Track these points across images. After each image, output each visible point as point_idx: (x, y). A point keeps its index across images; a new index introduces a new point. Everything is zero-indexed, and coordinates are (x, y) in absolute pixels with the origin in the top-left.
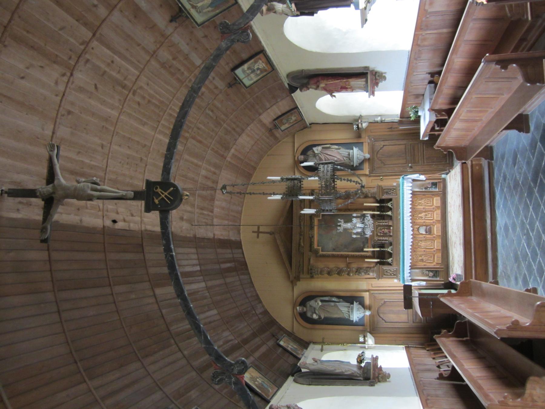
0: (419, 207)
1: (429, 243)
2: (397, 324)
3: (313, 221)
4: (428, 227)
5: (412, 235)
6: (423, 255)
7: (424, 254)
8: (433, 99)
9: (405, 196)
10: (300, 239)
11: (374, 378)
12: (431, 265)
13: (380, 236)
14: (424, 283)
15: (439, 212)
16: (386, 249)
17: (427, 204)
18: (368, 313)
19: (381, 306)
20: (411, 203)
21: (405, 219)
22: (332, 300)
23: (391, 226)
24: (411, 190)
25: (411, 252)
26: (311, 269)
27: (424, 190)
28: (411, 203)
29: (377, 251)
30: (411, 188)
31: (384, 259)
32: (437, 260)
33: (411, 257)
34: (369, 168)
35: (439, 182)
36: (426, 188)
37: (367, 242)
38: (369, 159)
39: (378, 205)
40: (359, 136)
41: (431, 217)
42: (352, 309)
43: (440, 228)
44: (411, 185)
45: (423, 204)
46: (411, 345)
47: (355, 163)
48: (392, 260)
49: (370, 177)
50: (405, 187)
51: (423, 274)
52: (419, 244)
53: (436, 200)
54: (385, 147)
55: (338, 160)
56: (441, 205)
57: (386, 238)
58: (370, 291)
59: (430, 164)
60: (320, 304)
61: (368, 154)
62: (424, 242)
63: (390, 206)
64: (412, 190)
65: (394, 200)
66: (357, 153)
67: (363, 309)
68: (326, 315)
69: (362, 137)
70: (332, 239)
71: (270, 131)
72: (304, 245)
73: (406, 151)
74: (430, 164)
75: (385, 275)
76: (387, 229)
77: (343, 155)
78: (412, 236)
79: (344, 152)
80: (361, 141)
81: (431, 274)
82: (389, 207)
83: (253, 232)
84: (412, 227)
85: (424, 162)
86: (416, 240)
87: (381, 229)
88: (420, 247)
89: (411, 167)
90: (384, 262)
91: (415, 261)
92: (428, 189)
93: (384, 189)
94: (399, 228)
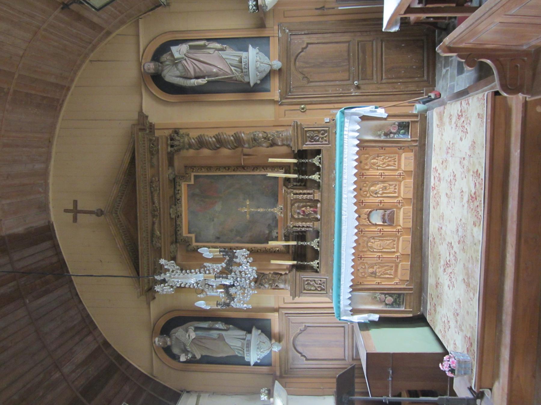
0: (372, 172)
1: (388, 242)
3: (178, 188)
4: (388, 212)
6: (376, 264)
7: (379, 263)
8: (177, 280)
9: (346, 151)
10: (153, 223)
12: (386, 284)
13: (298, 220)
14: (375, 317)
15: (410, 181)
16: (309, 243)
17: (388, 165)
18: (276, 348)
21: (344, 196)
22: (214, 327)
23: (318, 201)
24: (358, 138)
27: (383, 138)
29: (293, 245)
30: (357, 134)
32: (402, 275)
33: (353, 270)
34: (279, 89)
35: (412, 121)
36: (386, 135)
37: (276, 226)
38: (280, 70)
39: (295, 161)
40: (262, 25)
41: (395, 192)
42: (248, 345)
43: (411, 214)
44: (358, 127)
48: (318, 263)
49: (280, 105)
50: (345, 133)
51: (374, 300)
52: (369, 244)
53: (406, 158)
54: (309, 46)
55: (221, 73)
56: (415, 169)
57: (308, 224)
58: (280, 310)
59: (394, 81)
60: (193, 335)
61: (279, 60)
62: (380, 240)
63: (317, 164)
64: (359, 138)
65: (324, 152)
69: (267, 26)
70: (213, 221)
71: (62, 8)
72: (160, 233)
73: (349, 55)
74: (394, 81)
75: (305, 289)
76: (311, 207)
77: (228, 62)
78: (356, 231)
83: (66, 211)
84: (356, 211)
85: (382, 77)
86: (363, 236)
87: (299, 208)
88: (371, 249)
89: (358, 87)
91: (360, 276)
92: (392, 135)
93: (306, 131)
94: (333, 206)
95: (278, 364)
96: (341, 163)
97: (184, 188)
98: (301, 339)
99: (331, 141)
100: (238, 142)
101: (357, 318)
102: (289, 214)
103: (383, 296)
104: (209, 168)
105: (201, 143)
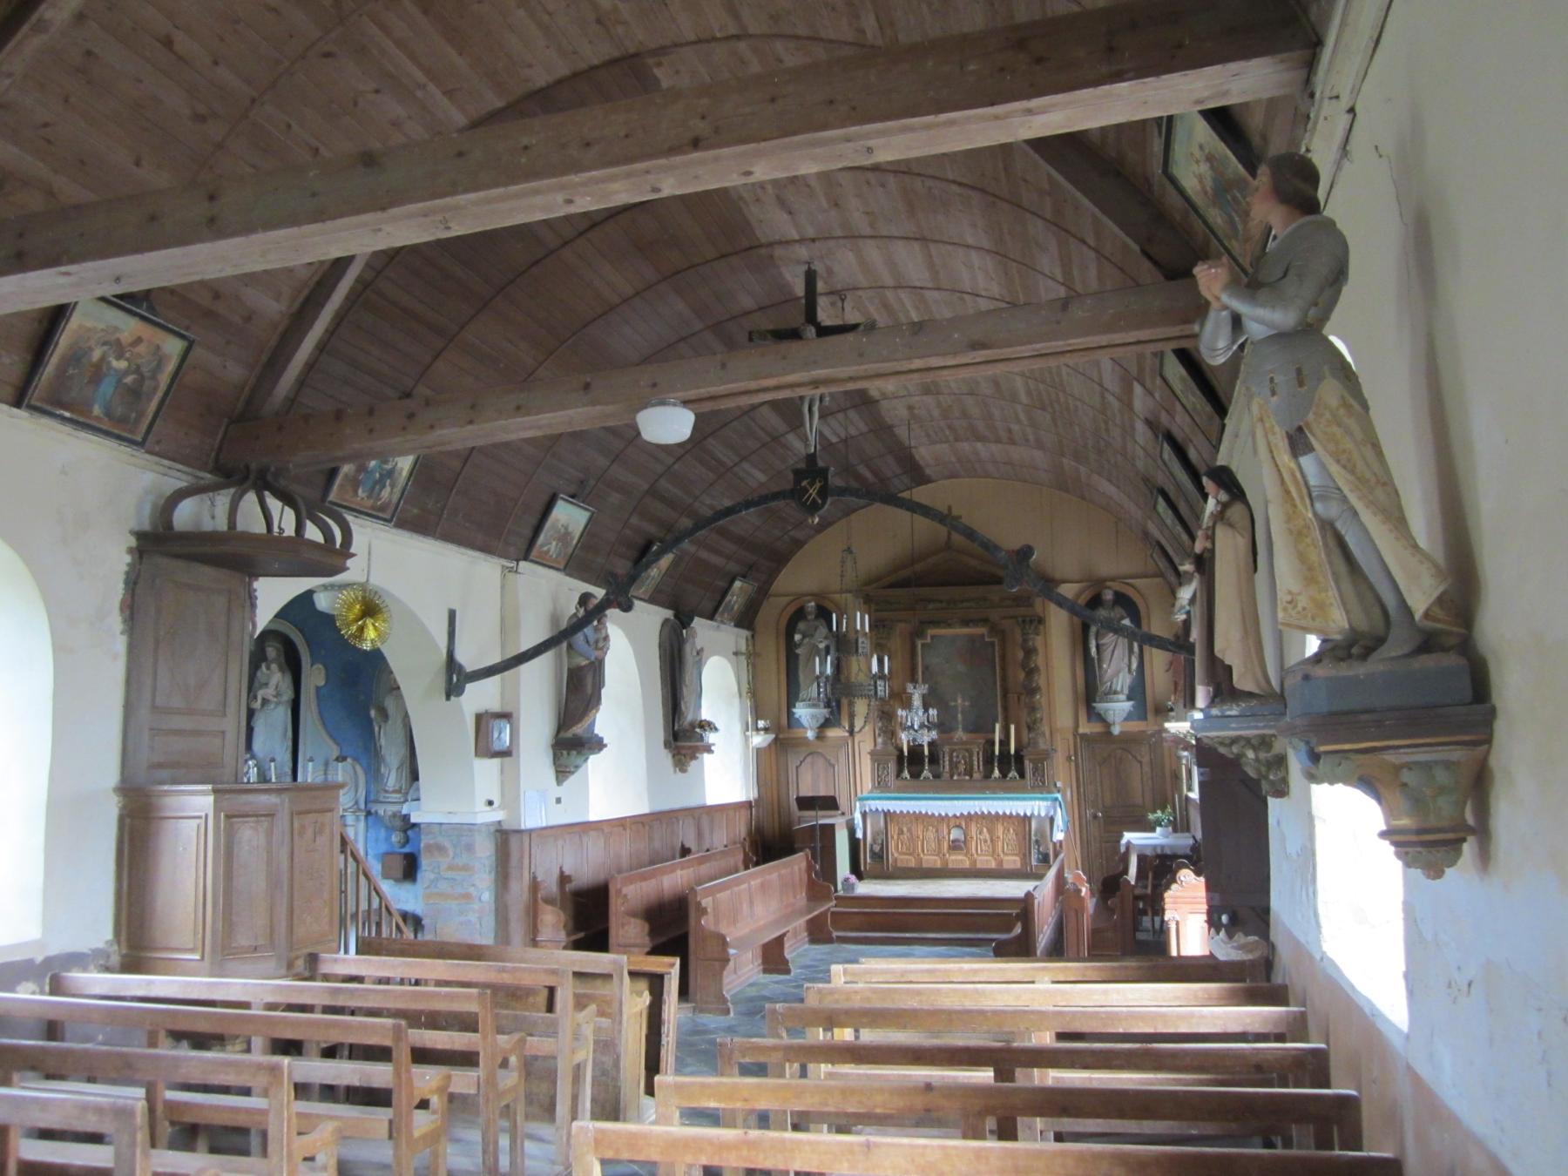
2: (795, 785)
5: (947, 815)
6: (911, 834)
11: (677, 747)
12: (892, 845)
14: (859, 835)
15: (993, 865)
18: (810, 734)
19: (826, 759)
20: (1008, 813)
21: (977, 802)
23: (971, 776)
24: (1032, 814)
25: (915, 812)
26: (884, 626)
27: (1033, 838)
28: (1008, 813)
30: (1036, 813)
31: (909, 764)
32: (902, 860)
36: (1037, 842)
39: (1012, 751)
42: (814, 706)
43: (961, 866)
44: (1043, 814)
45: (1007, 838)
46: (757, 812)
47: (1100, 706)
50: (1037, 802)
52: (931, 828)
57: (947, 768)
63: (1010, 775)
65: (1022, 782)
66: (1118, 709)
67: (818, 725)
68: (801, 658)
74: (1104, 855)
75: (878, 765)
76: (965, 769)
77: (1115, 680)
79: (1123, 681)
80: (1150, 716)
81: (877, 848)
82: (1009, 771)
84: (962, 814)
88: (926, 829)
89: (1095, 817)
90: (903, 764)
95: (792, 736)
96: (1008, 799)
97: (981, 630)
98: (820, 762)
99: (1034, 789)
100: (1032, 691)
101: (858, 817)
102: (956, 747)
103: (880, 842)
104: (1003, 658)
105: (1030, 652)
